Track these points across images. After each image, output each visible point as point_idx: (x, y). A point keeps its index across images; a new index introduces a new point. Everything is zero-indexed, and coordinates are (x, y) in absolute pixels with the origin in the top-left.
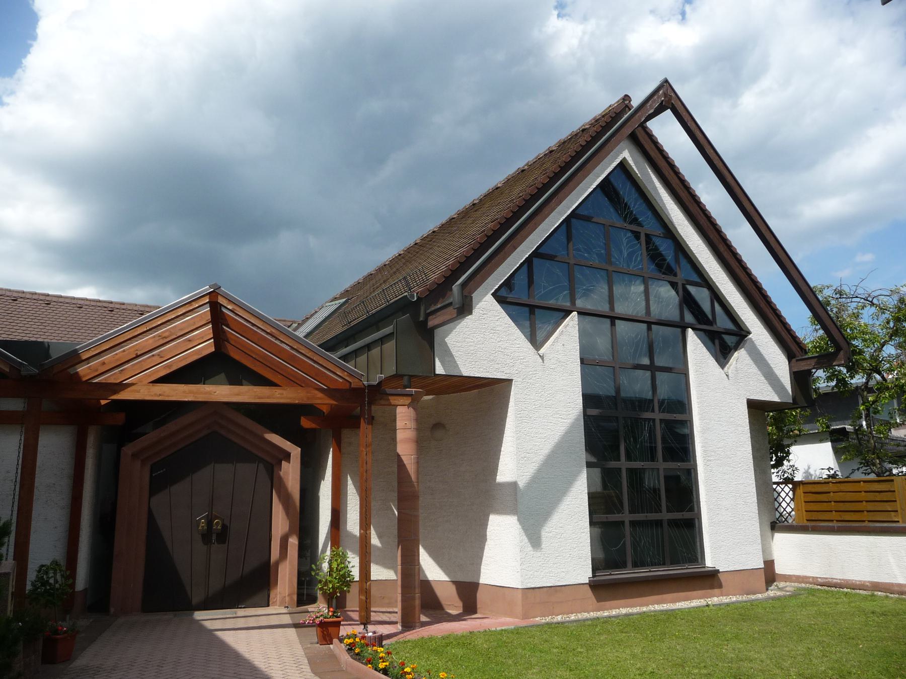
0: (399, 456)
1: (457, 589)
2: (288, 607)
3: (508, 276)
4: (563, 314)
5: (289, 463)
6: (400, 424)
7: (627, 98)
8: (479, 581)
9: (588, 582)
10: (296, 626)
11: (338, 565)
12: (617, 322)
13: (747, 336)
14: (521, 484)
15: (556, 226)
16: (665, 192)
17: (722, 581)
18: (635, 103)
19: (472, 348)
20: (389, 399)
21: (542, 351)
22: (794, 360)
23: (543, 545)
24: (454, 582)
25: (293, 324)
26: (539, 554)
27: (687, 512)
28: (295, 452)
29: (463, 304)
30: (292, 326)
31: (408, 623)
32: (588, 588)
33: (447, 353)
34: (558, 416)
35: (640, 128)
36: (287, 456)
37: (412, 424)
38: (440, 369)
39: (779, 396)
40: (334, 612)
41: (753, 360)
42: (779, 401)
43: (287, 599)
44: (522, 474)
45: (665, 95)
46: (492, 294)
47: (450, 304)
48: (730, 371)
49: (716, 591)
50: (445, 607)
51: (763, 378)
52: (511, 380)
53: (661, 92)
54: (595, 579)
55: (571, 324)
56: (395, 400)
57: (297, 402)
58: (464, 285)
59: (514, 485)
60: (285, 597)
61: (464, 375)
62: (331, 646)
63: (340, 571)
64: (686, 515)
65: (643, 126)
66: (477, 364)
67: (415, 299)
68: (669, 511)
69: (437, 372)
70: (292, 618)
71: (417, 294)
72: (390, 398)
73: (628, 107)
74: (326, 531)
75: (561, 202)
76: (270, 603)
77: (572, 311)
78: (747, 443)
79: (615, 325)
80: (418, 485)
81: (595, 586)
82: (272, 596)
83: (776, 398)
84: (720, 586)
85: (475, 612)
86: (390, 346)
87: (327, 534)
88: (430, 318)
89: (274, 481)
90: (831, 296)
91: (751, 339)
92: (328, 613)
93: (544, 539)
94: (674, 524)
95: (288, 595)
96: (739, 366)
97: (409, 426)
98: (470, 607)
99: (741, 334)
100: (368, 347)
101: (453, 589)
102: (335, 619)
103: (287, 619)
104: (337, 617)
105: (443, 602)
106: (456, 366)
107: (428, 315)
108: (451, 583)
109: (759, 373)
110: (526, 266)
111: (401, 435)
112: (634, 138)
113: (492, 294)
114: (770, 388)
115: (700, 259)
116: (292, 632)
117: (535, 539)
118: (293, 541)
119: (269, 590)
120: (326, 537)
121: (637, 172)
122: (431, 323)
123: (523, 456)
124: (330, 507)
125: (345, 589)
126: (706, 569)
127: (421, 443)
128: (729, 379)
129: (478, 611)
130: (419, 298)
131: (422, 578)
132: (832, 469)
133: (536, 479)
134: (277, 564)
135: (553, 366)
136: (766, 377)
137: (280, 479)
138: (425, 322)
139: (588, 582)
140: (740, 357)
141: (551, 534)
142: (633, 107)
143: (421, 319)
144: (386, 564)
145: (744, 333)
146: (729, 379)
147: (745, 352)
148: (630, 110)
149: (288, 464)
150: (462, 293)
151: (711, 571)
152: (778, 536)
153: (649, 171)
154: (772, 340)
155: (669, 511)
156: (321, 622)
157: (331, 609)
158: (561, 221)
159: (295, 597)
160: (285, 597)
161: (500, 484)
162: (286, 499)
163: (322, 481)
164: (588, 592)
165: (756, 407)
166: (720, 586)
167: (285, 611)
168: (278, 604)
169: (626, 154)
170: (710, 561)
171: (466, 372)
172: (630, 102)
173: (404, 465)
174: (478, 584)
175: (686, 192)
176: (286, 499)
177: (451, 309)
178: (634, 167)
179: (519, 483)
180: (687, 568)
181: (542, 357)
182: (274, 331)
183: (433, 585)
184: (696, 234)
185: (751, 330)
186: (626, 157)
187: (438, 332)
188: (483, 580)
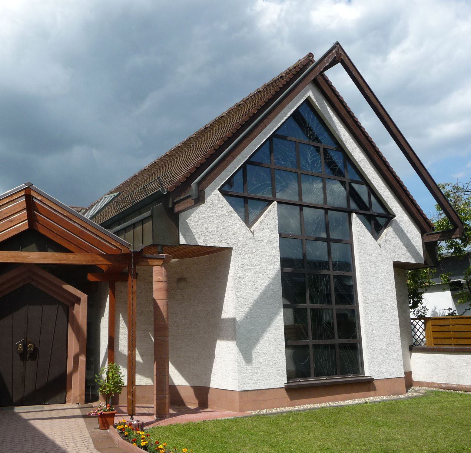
0: (154, 300)
1: (195, 391)
2: (78, 404)
3: (229, 177)
4: (268, 203)
5: (80, 305)
6: (155, 278)
7: (311, 55)
8: (210, 386)
9: (284, 387)
10: (84, 417)
11: (113, 375)
12: (304, 208)
13: (393, 218)
14: (238, 320)
15: (262, 143)
16: (337, 119)
17: (376, 386)
18: (317, 58)
19: (205, 226)
20: (148, 262)
21: (253, 228)
22: (425, 235)
23: (253, 361)
24: (194, 387)
25: (82, 210)
26: (250, 367)
27: (352, 338)
28: (84, 297)
29: (199, 197)
30: (81, 211)
31: (161, 415)
32: (284, 390)
33: (188, 229)
34: (263, 273)
35: (320, 76)
36: (78, 300)
37: (164, 279)
38: (183, 241)
39: (415, 259)
40: (110, 407)
41: (397, 234)
42: (415, 262)
43: (78, 398)
44: (239, 313)
45: (337, 53)
46: (219, 190)
47: (190, 196)
48: (381, 242)
49: (372, 393)
50: (186, 404)
51: (404, 247)
52: (232, 248)
53: (334, 51)
54: (289, 384)
55: (272, 210)
56: (152, 262)
57: (85, 263)
58: (199, 183)
59: (234, 320)
60: (77, 397)
61: (199, 245)
62: (108, 430)
63: (114, 379)
64: (351, 341)
65: (322, 74)
66: (208, 237)
67: (166, 192)
68: (339, 338)
69: (181, 243)
70: (82, 412)
71: (167, 189)
72: (149, 260)
73: (312, 61)
74: (105, 352)
75: (234, 158)
76: (67, 401)
77: (273, 201)
78: (393, 291)
79: (302, 211)
80: (168, 320)
81: (289, 389)
82: (67, 396)
83: (413, 261)
84: (374, 389)
85: (207, 407)
86: (149, 225)
87: (106, 354)
88: (176, 205)
89: (69, 317)
90: (451, 190)
91: (396, 220)
92: (106, 408)
93: (254, 357)
94: (344, 347)
95: (79, 396)
96: (387, 238)
97: (161, 280)
98: (203, 404)
99: (389, 216)
100: (134, 225)
101: (192, 391)
102: (111, 412)
103: (78, 412)
104: (112, 410)
105: (185, 400)
106: (194, 239)
107: (175, 204)
108: (190, 388)
109: (401, 243)
110: (268, 142)
111: (156, 286)
112: (315, 82)
113: (219, 190)
114: (409, 254)
115: (361, 165)
116: (81, 421)
117: (248, 357)
118: (82, 359)
119: (66, 392)
120: (105, 356)
121: (318, 106)
122: (177, 209)
123: (239, 300)
124: (108, 335)
125: (118, 391)
126: (365, 378)
127: (170, 291)
128: (381, 248)
129: (209, 406)
130: (168, 192)
131: (170, 384)
132: (451, 309)
133: (248, 316)
134: (71, 374)
135: (260, 239)
136: (406, 247)
137: (73, 316)
138: (173, 208)
139: (284, 387)
140: (388, 233)
141: (259, 354)
142: (315, 61)
143: (170, 206)
144: (146, 374)
145: (391, 216)
146: (381, 248)
147: (392, 229)
148: (313, 63)
149: (79, 306)
150: (198, 189)
151: (369, 379)
152: (415, 355)
153: (326, 105)
154: (410, 221)
155: (339, 338)
156: (101, 414)
157: (108, 405)
158: (265, 139)
159: (84, 397)
160: (77, 397)
161: (224, 319)
162: (77, 330)
163: (102, 318)
164: (285, 394)
165: (399, 267)
166: (374, 389)
167: (77, 406)
168: (72, 401)
169: (310, 93)
170: (368, 373)
171: (201, 242)
172: (313, 57)
173: (158, 307)
174: (209, 388)
175: (351, 119)
176: (77, 330)
177: (190, 199)
178: (316, 102)
179: (237, 319)
180: (352, 377)
181: (253, 233)
182: (69, 214)
183: (178, 388)
184: (358, 148)
185: (396, 214)
186: (310, 96)
187: (182, 216)
188: (212, 386)
